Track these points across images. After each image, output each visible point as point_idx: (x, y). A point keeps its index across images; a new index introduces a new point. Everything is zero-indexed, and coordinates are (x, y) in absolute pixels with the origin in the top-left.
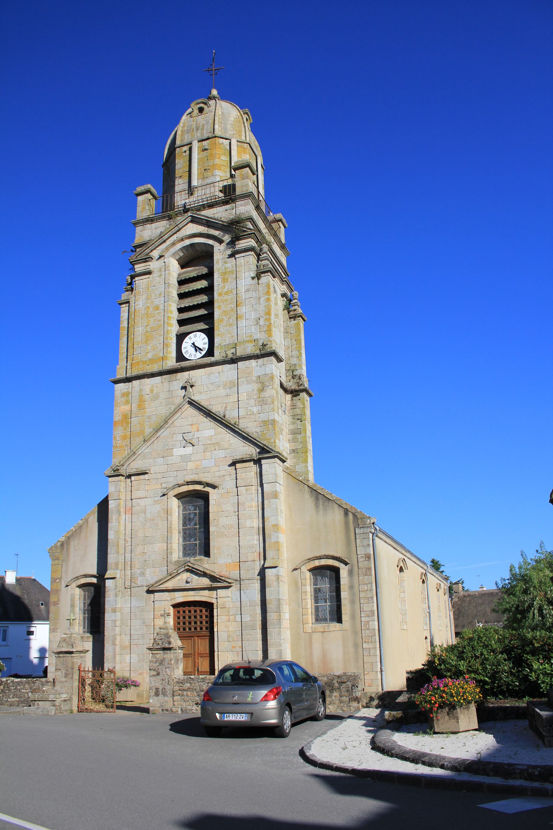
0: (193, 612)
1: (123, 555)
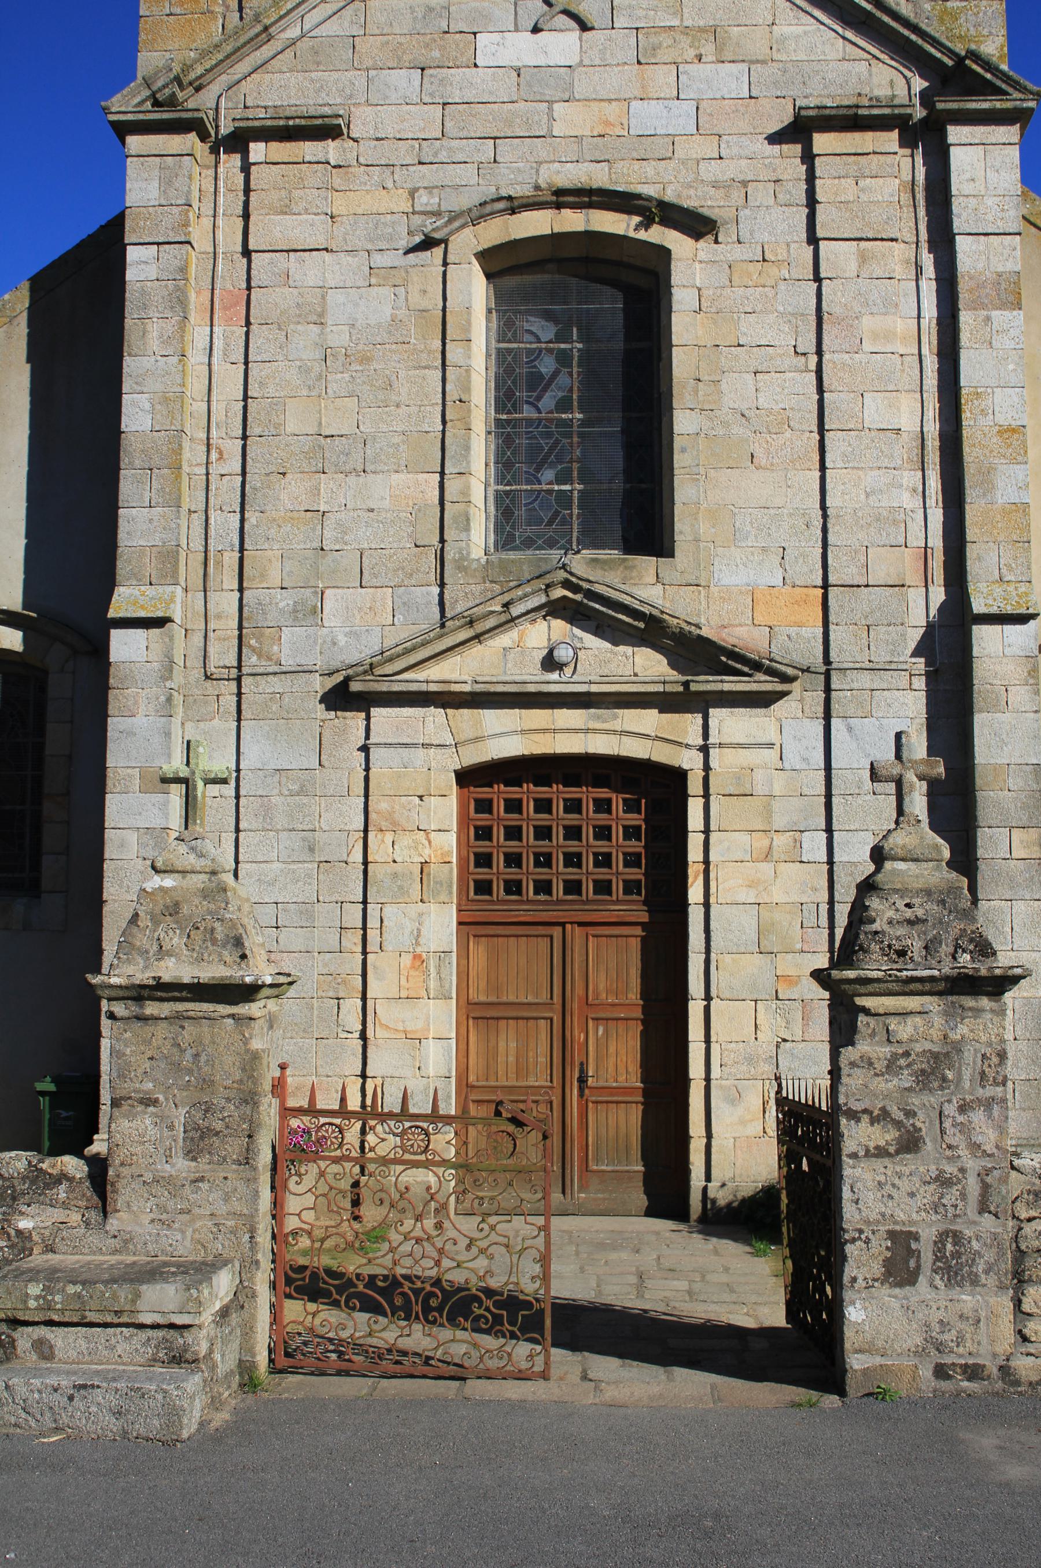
0: (558, 807)
1: (198, 520)
